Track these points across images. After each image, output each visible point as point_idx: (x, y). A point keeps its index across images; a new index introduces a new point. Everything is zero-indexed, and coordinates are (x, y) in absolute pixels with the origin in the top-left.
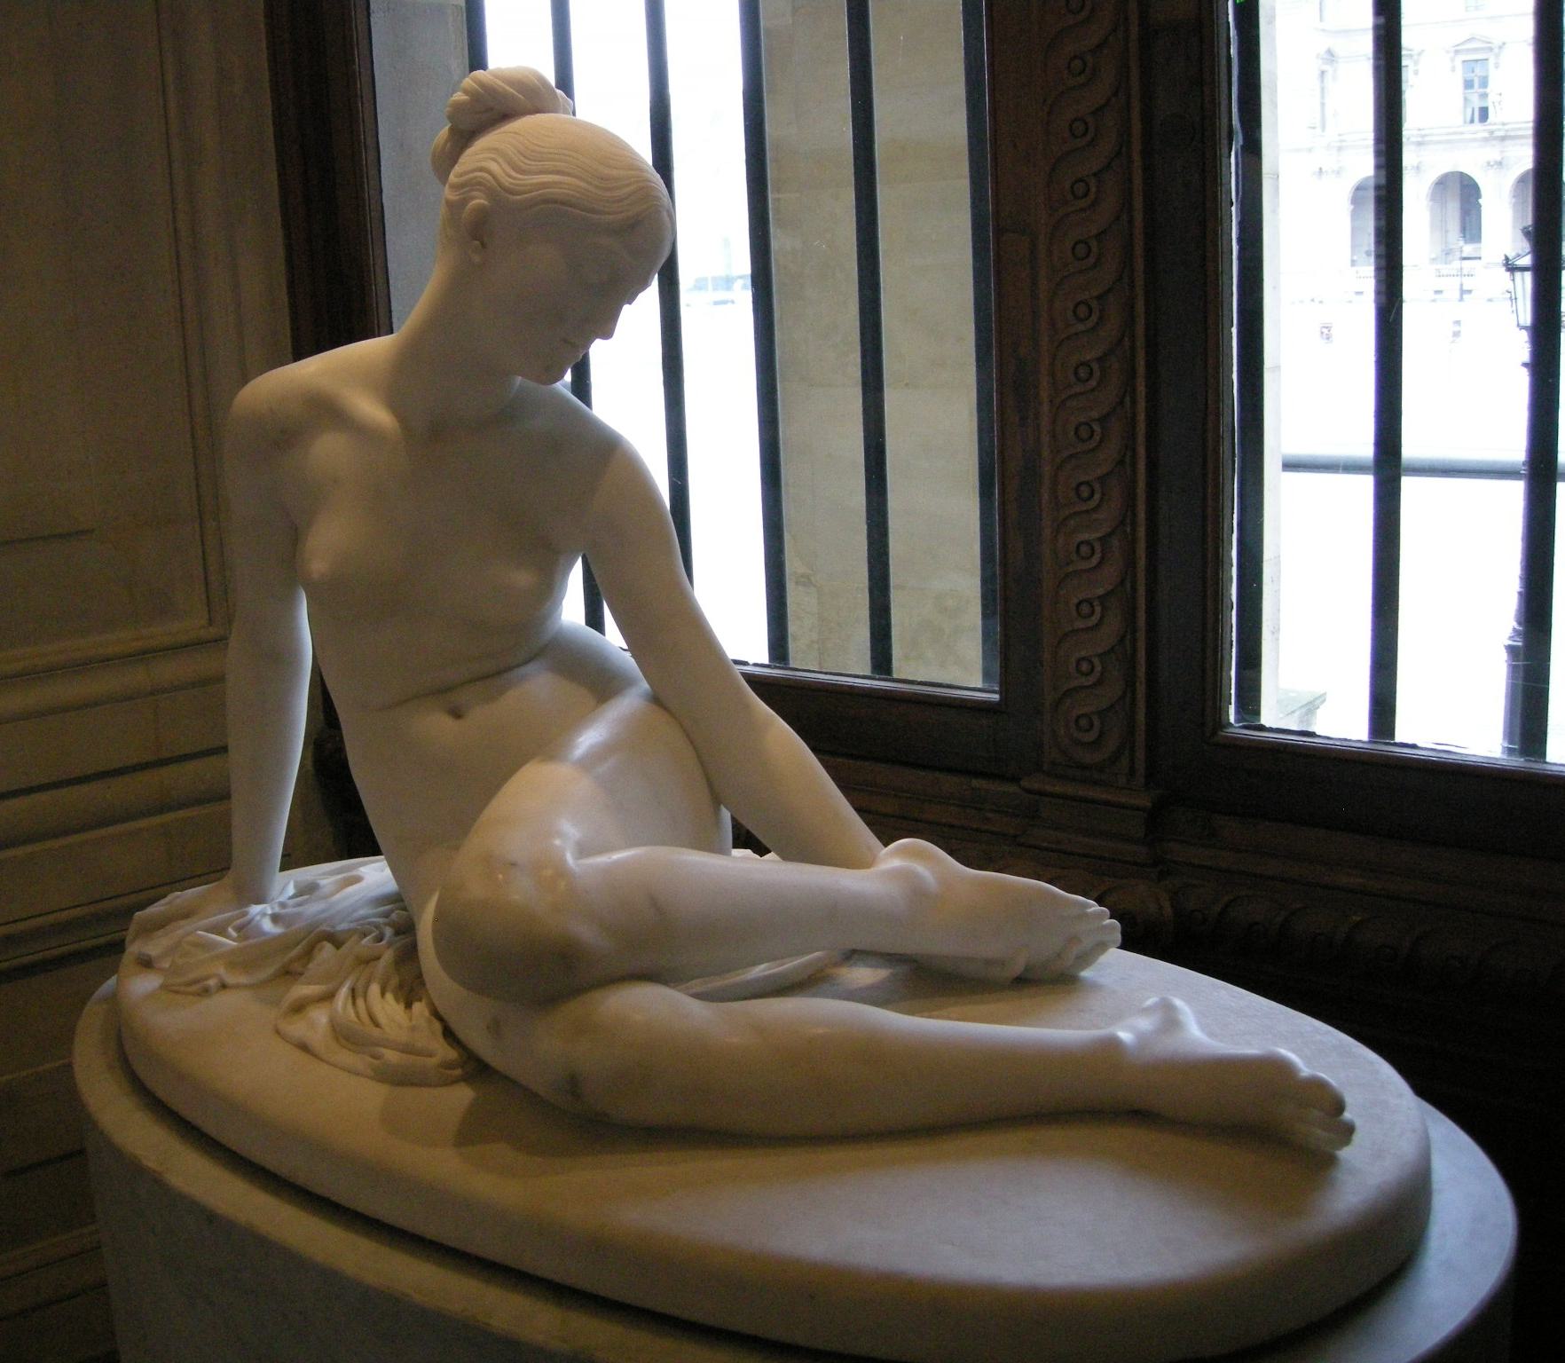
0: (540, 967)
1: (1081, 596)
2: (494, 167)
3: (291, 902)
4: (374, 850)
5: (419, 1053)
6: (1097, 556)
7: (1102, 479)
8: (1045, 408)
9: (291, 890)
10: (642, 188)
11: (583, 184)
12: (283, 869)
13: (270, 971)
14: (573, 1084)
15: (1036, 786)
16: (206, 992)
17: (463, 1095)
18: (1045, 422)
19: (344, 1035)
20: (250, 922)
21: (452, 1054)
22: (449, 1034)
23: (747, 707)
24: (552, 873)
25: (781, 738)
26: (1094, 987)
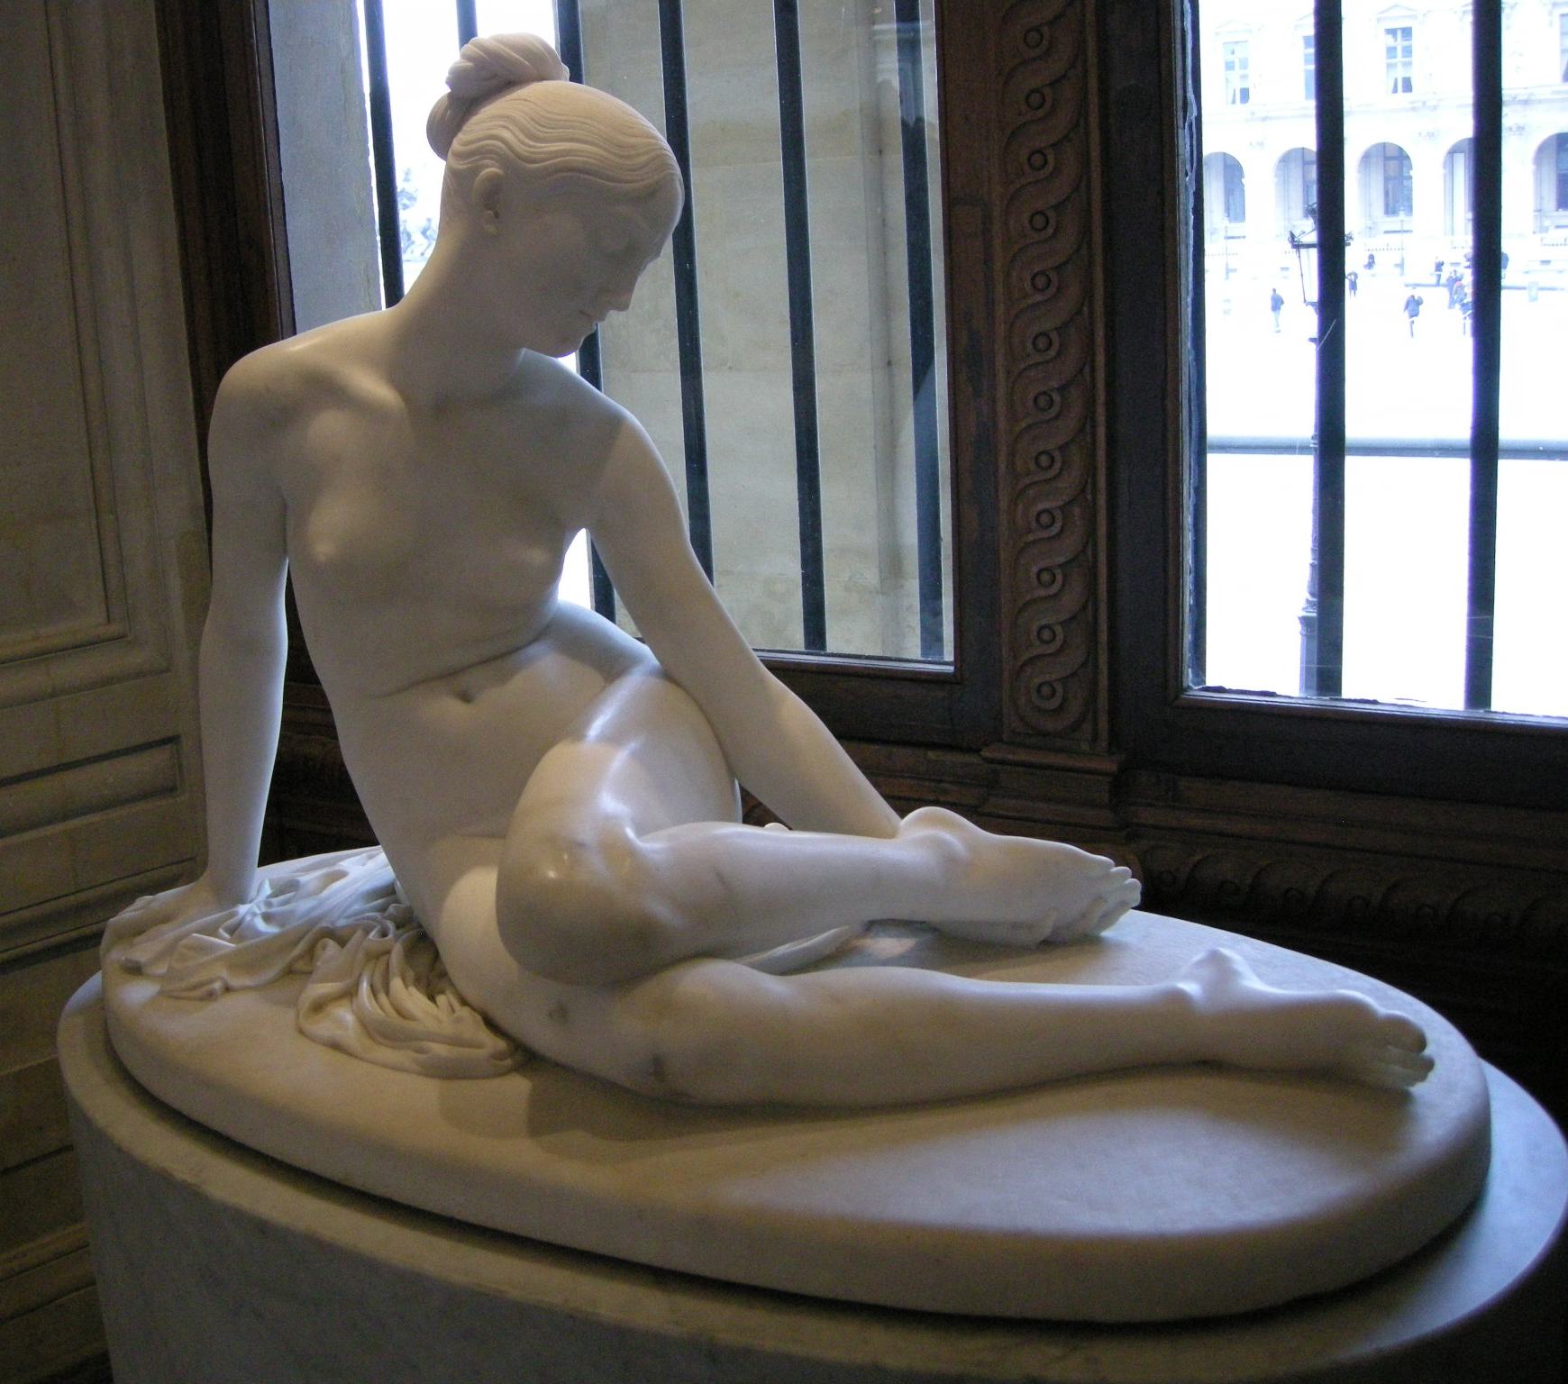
0: (606, 943)
1: (1043, 564)
2: (506, 134)
3: (275, 900)
4: (368, 840)
5: (470, 1045)
6: (1058, 525)
7: (1063, 448)
8: (1001, 376)
9: (267, 890)
10: (658, 156)
11: (594, 149)
12: (262, 862)
13: (271, 973)
14: (658, 1066)
15: (998, 756)
16: (211, 996)
17: (519, 1087)
18: (1001, 392)
19: (376, 1031)
20: (240, 924)
21: (501, 1044)
22: (491, 1024)
23: (762, 681)
24: (617, 850)
25: (798, 717)
26: (1120, 946)
